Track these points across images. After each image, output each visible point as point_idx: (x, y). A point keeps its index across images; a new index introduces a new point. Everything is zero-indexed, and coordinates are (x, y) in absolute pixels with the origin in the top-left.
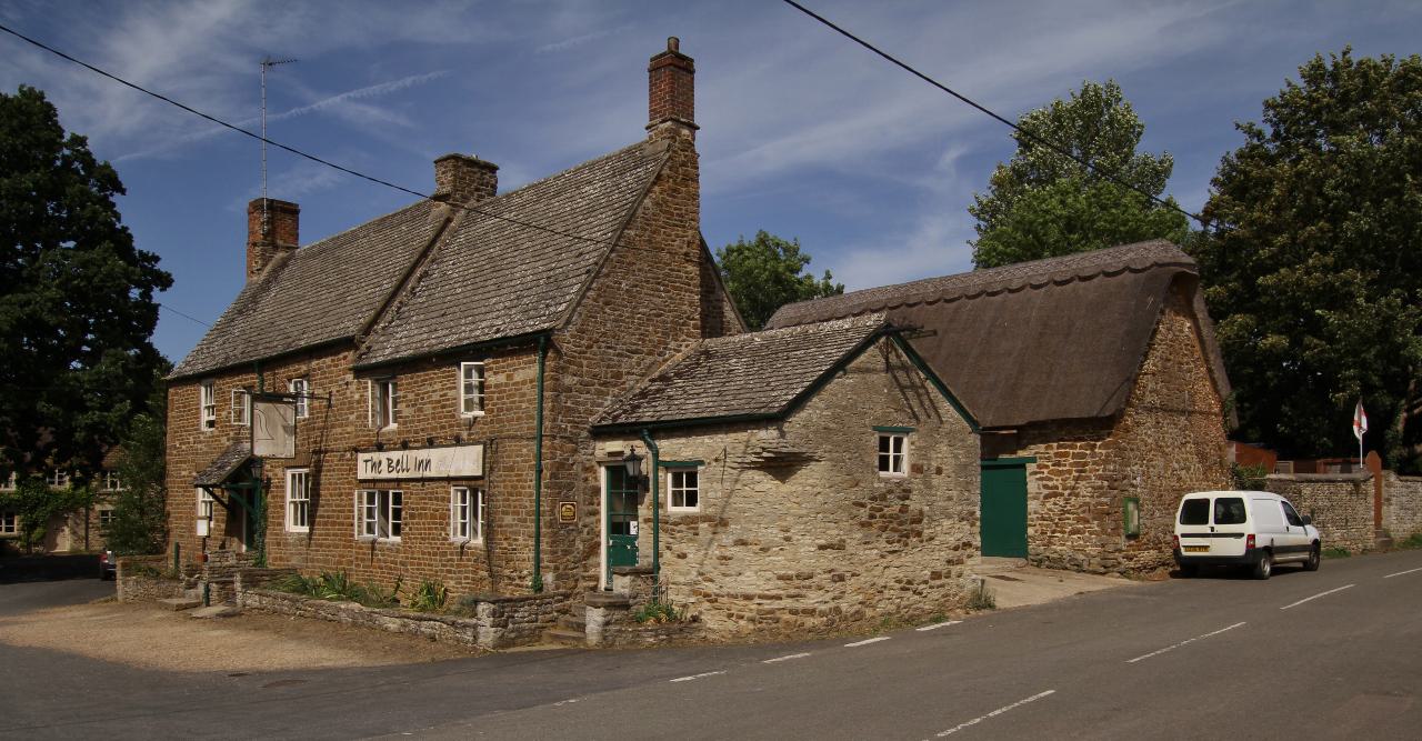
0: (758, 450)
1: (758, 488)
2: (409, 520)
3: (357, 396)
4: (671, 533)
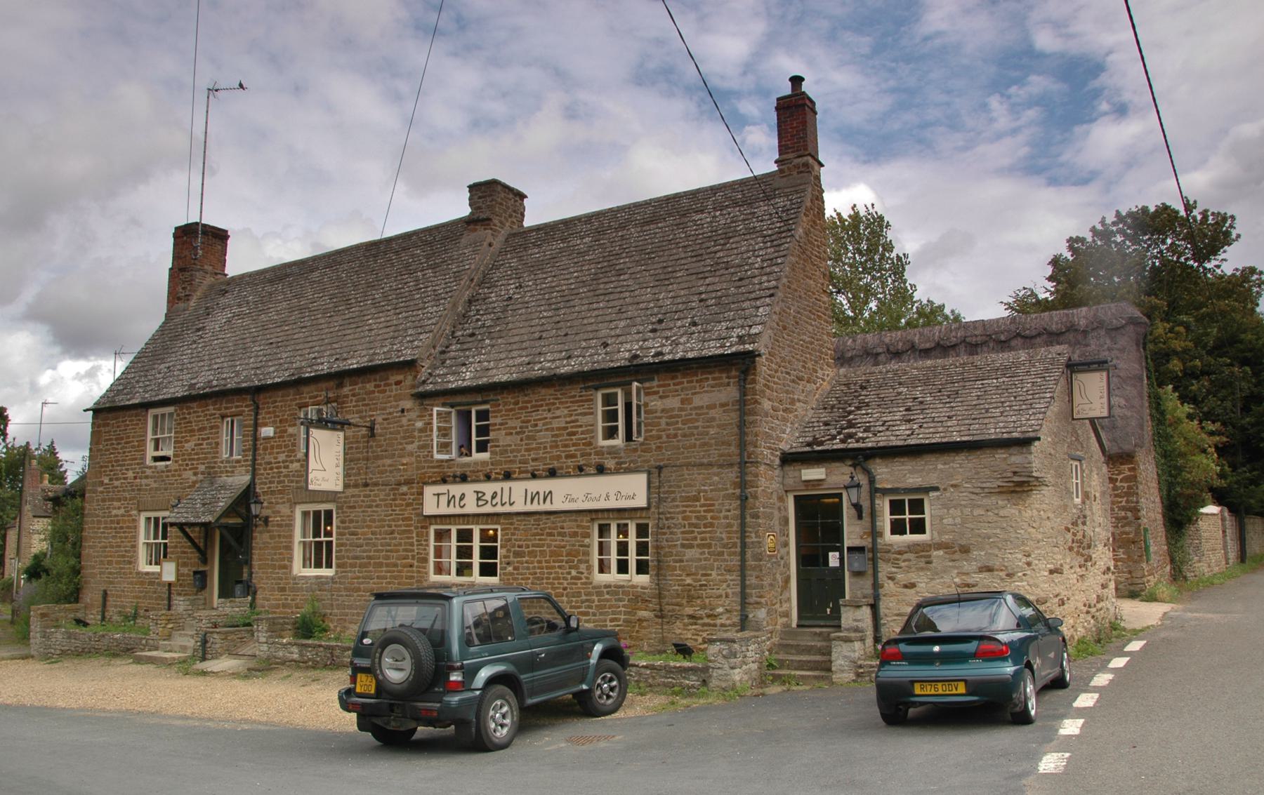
0: (1009, 475)
1: (1002, 513)
2: (512, 559)
3: (419, 424)
4: (895, 563)
